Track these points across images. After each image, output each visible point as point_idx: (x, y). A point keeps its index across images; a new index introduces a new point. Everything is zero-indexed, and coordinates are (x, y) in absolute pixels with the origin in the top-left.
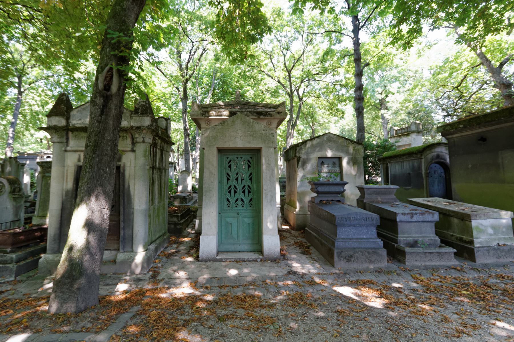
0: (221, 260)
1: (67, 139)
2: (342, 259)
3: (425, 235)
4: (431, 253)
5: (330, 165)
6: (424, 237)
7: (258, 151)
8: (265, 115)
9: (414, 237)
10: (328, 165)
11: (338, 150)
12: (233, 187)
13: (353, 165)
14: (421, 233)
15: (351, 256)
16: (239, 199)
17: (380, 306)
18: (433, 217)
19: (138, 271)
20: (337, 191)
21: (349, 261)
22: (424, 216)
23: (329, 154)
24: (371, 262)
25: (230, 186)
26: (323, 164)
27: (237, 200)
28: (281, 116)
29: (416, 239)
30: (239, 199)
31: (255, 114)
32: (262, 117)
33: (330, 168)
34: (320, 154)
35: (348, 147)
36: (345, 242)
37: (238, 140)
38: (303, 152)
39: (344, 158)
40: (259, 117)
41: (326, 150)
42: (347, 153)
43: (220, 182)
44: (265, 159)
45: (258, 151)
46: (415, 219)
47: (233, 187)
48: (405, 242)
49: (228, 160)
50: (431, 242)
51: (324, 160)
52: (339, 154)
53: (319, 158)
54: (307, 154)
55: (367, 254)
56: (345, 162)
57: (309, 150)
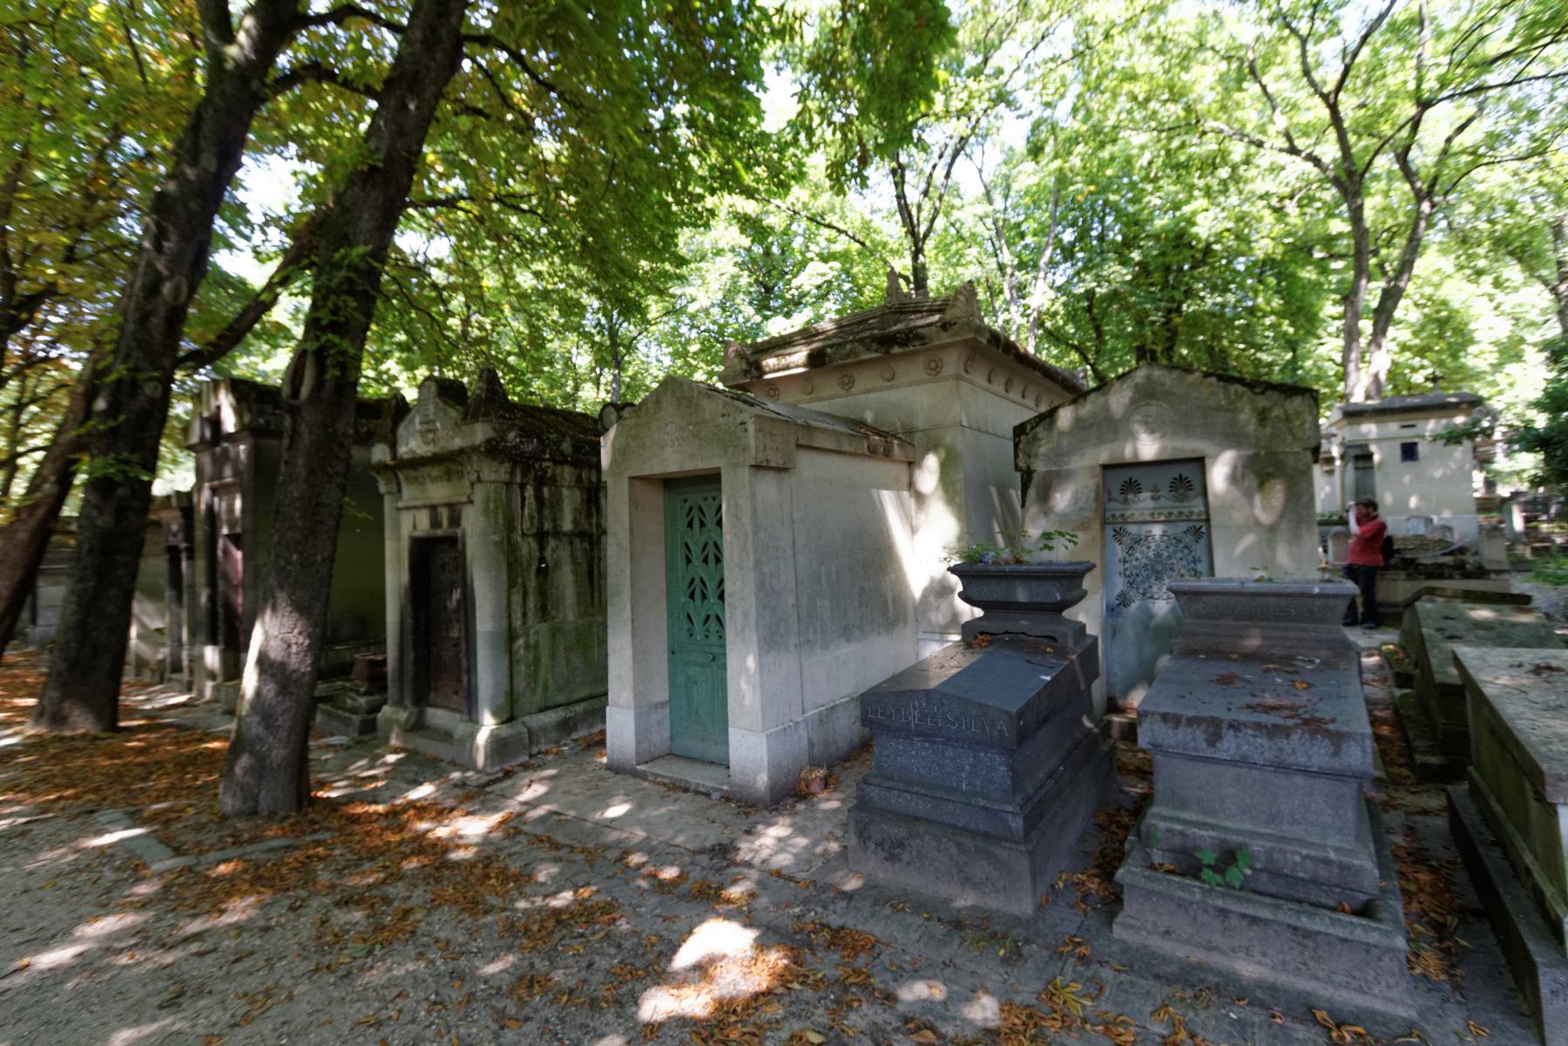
0: (643, 776)
1: (399, 485)
2: (872, 846)
3: (1298, 831)
4: (1254, 920)
5: (1164, 492)
6: (1282, 839)
7: (711, 479)
8: (903, 344)
9: (1227, 830)
10: (1155, 489)
11: (1184, 425)
12: (697, 582)
13: (1261, 485)
14: (1273, 819)
15: (901, 845)
16: (713, 617)
17: (252, 912)
18: (1336, 753)
19: (480, 760)
20: (1001, 598)
21: (892, 858)
22: (1283, 743)
23: (1148, 447)
24: (966, 881)
25: (692, 581)
26: (1131, 487)
27: (708, 618)
28: (956, 334)
29: (1235, 839)
30: (713, 617)
31: (874, 346)
32: (896, 350)
33: (1163, 502)
34: (1104, 455)
35: (1234, 411)
36: (888, 788)
37: (668, 452)
38: (1042, 450)
39: (1215, 457)
40: (887, 352)
41: (1132, 436)
42: (1232, 438)
43: (670, 569)
44: (728, 502)
45: (711, 479)
46: (1229, 745)
47: (697, 582)
48: (1177, 841)
49: (687, 506)
50: (1323, 872)
51: (1135, 474)
52: (1190, 446)
53: (1106, 467)
54: (1058, 455)
55: (954, 850)
56: (1219, 474)
57: (1065, 442)
